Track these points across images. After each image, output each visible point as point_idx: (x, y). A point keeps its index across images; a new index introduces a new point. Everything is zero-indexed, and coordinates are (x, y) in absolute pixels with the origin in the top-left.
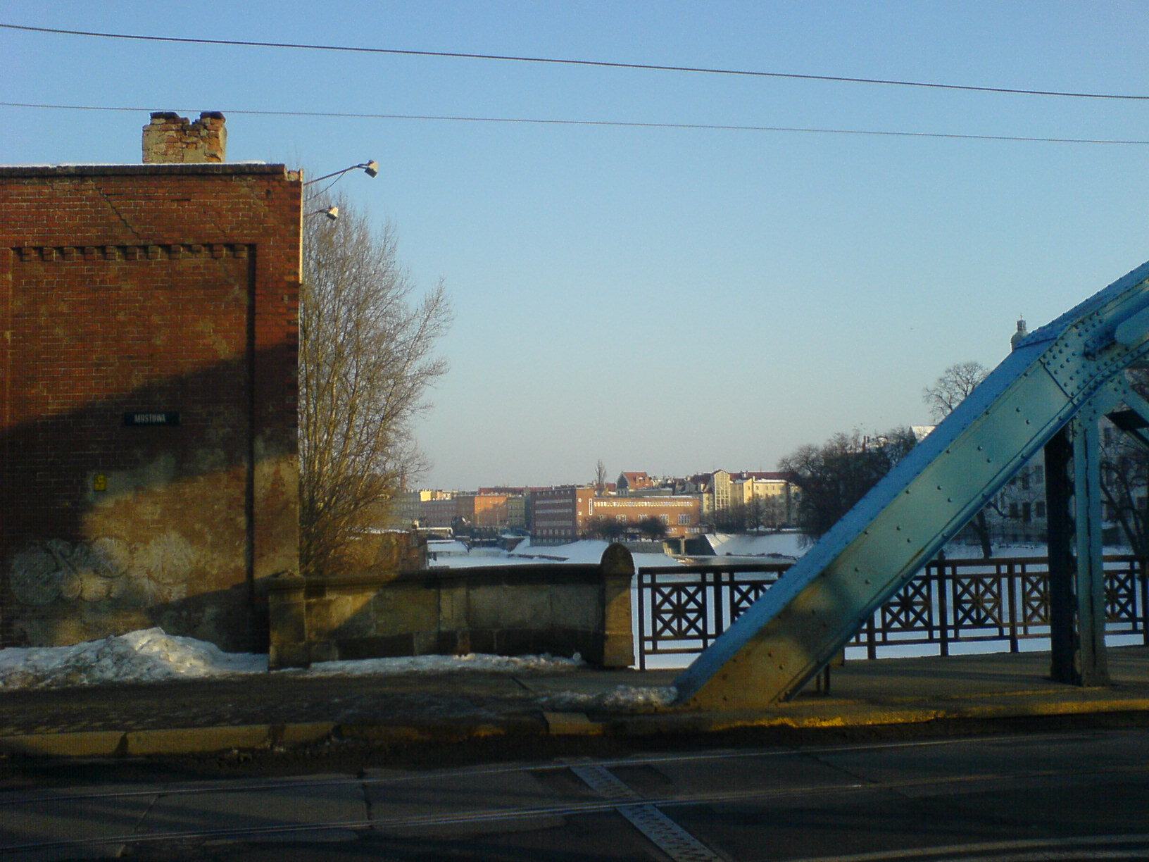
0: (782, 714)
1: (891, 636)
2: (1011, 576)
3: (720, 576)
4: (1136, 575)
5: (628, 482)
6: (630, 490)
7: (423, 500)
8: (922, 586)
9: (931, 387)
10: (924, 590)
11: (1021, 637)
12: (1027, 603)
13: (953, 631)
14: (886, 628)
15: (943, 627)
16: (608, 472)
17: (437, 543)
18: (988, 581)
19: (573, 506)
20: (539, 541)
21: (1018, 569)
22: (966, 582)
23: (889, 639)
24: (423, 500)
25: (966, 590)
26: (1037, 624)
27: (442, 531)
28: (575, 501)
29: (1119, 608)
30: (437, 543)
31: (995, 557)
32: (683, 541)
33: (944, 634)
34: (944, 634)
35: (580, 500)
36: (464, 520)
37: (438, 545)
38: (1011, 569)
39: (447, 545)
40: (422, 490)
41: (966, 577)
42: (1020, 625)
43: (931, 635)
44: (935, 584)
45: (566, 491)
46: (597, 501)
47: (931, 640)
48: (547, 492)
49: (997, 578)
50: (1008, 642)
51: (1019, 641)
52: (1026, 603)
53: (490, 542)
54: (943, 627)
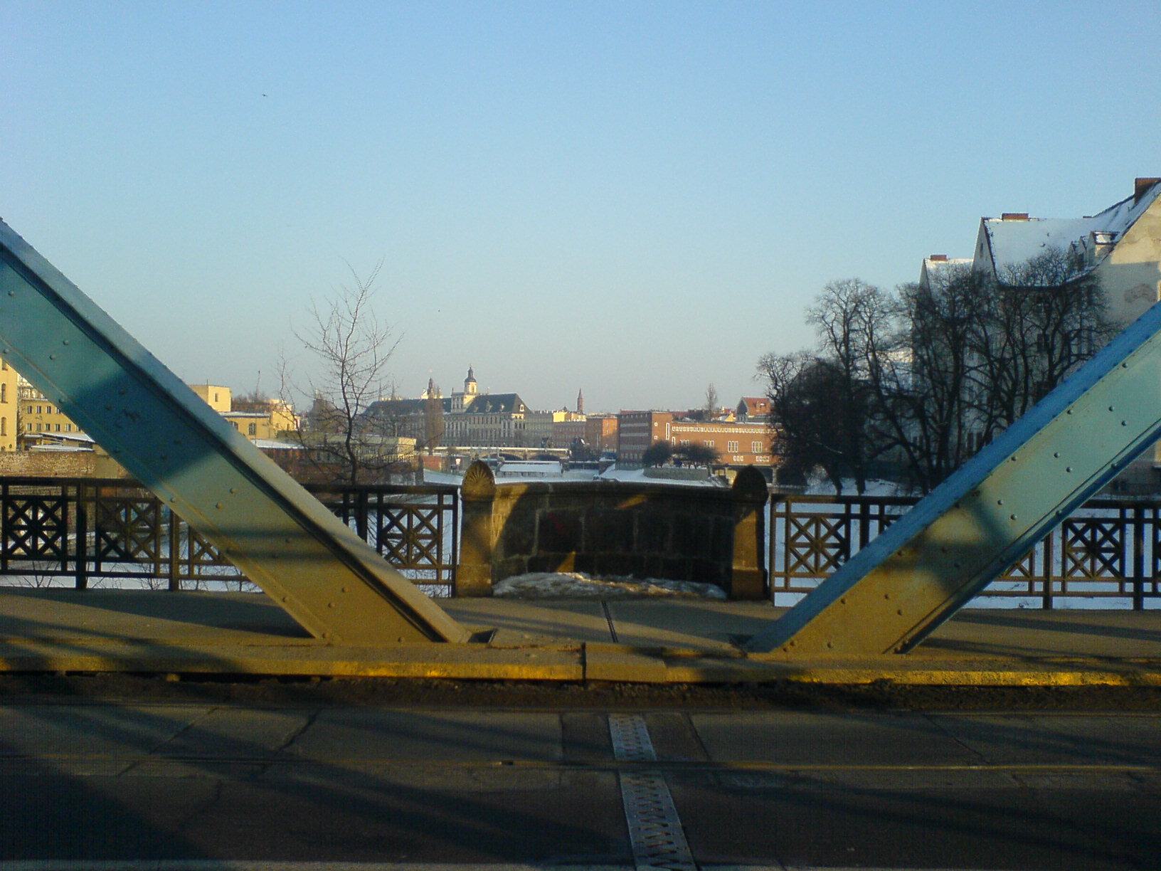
0: (890, 667)
1: (1071, 587)
2: (865, 518)
3: (868, 509)
4: (351, 511)
5: (748, 407)
6: (750, 416)
7: (555, 420)
8: (1113, 530)
9: (820, 294)
10: (1117, 536)
11: (1148, 595)
12: (791, 549)
13: (1060, 584)
14: (193, 561)
15: (1138, 579)
16: (718, 397)
17: (535, 464)
18: (833, 522)
19: (649, 430)
20: (622, 464)
21: (874, 510)
22: (803, 522)
23: (102, 570)
24: (555, 420)
25: (802, 530)
26: (1078, 580)
27: (560, 452)
28: (651, 425)
29: (43, 542)
30: (535, 464)
31: (868, 495)
32: (774, 471)
33: (1138, 587)
34: (1138, 587)
35: (656, 424)
36: (583, 441)
37: (537, 465)
38: (865, 510)
39: (518, 465)
40: (556, 412)
41: (803, 515)
42: (1056, 579)
43: (439, 575)
44: (1130, 528)
45: (244, 408)
46: (676, 425)
47: (1122, 593)
48: (629, 415)
49: (845, 519)
50: (1131, 600)
51: (776, 594)
52: (1066, 554)
53: (576, 464)
54: (1138, 579)
